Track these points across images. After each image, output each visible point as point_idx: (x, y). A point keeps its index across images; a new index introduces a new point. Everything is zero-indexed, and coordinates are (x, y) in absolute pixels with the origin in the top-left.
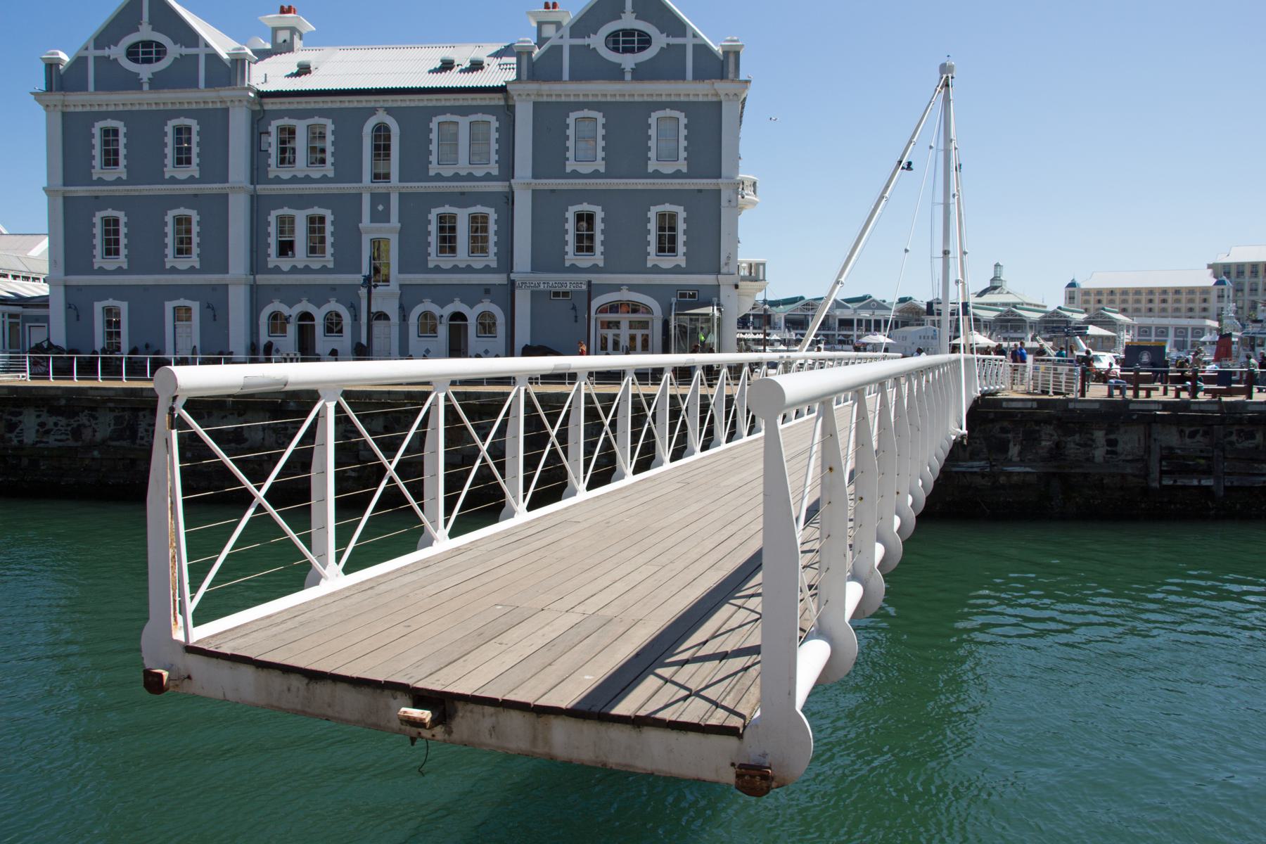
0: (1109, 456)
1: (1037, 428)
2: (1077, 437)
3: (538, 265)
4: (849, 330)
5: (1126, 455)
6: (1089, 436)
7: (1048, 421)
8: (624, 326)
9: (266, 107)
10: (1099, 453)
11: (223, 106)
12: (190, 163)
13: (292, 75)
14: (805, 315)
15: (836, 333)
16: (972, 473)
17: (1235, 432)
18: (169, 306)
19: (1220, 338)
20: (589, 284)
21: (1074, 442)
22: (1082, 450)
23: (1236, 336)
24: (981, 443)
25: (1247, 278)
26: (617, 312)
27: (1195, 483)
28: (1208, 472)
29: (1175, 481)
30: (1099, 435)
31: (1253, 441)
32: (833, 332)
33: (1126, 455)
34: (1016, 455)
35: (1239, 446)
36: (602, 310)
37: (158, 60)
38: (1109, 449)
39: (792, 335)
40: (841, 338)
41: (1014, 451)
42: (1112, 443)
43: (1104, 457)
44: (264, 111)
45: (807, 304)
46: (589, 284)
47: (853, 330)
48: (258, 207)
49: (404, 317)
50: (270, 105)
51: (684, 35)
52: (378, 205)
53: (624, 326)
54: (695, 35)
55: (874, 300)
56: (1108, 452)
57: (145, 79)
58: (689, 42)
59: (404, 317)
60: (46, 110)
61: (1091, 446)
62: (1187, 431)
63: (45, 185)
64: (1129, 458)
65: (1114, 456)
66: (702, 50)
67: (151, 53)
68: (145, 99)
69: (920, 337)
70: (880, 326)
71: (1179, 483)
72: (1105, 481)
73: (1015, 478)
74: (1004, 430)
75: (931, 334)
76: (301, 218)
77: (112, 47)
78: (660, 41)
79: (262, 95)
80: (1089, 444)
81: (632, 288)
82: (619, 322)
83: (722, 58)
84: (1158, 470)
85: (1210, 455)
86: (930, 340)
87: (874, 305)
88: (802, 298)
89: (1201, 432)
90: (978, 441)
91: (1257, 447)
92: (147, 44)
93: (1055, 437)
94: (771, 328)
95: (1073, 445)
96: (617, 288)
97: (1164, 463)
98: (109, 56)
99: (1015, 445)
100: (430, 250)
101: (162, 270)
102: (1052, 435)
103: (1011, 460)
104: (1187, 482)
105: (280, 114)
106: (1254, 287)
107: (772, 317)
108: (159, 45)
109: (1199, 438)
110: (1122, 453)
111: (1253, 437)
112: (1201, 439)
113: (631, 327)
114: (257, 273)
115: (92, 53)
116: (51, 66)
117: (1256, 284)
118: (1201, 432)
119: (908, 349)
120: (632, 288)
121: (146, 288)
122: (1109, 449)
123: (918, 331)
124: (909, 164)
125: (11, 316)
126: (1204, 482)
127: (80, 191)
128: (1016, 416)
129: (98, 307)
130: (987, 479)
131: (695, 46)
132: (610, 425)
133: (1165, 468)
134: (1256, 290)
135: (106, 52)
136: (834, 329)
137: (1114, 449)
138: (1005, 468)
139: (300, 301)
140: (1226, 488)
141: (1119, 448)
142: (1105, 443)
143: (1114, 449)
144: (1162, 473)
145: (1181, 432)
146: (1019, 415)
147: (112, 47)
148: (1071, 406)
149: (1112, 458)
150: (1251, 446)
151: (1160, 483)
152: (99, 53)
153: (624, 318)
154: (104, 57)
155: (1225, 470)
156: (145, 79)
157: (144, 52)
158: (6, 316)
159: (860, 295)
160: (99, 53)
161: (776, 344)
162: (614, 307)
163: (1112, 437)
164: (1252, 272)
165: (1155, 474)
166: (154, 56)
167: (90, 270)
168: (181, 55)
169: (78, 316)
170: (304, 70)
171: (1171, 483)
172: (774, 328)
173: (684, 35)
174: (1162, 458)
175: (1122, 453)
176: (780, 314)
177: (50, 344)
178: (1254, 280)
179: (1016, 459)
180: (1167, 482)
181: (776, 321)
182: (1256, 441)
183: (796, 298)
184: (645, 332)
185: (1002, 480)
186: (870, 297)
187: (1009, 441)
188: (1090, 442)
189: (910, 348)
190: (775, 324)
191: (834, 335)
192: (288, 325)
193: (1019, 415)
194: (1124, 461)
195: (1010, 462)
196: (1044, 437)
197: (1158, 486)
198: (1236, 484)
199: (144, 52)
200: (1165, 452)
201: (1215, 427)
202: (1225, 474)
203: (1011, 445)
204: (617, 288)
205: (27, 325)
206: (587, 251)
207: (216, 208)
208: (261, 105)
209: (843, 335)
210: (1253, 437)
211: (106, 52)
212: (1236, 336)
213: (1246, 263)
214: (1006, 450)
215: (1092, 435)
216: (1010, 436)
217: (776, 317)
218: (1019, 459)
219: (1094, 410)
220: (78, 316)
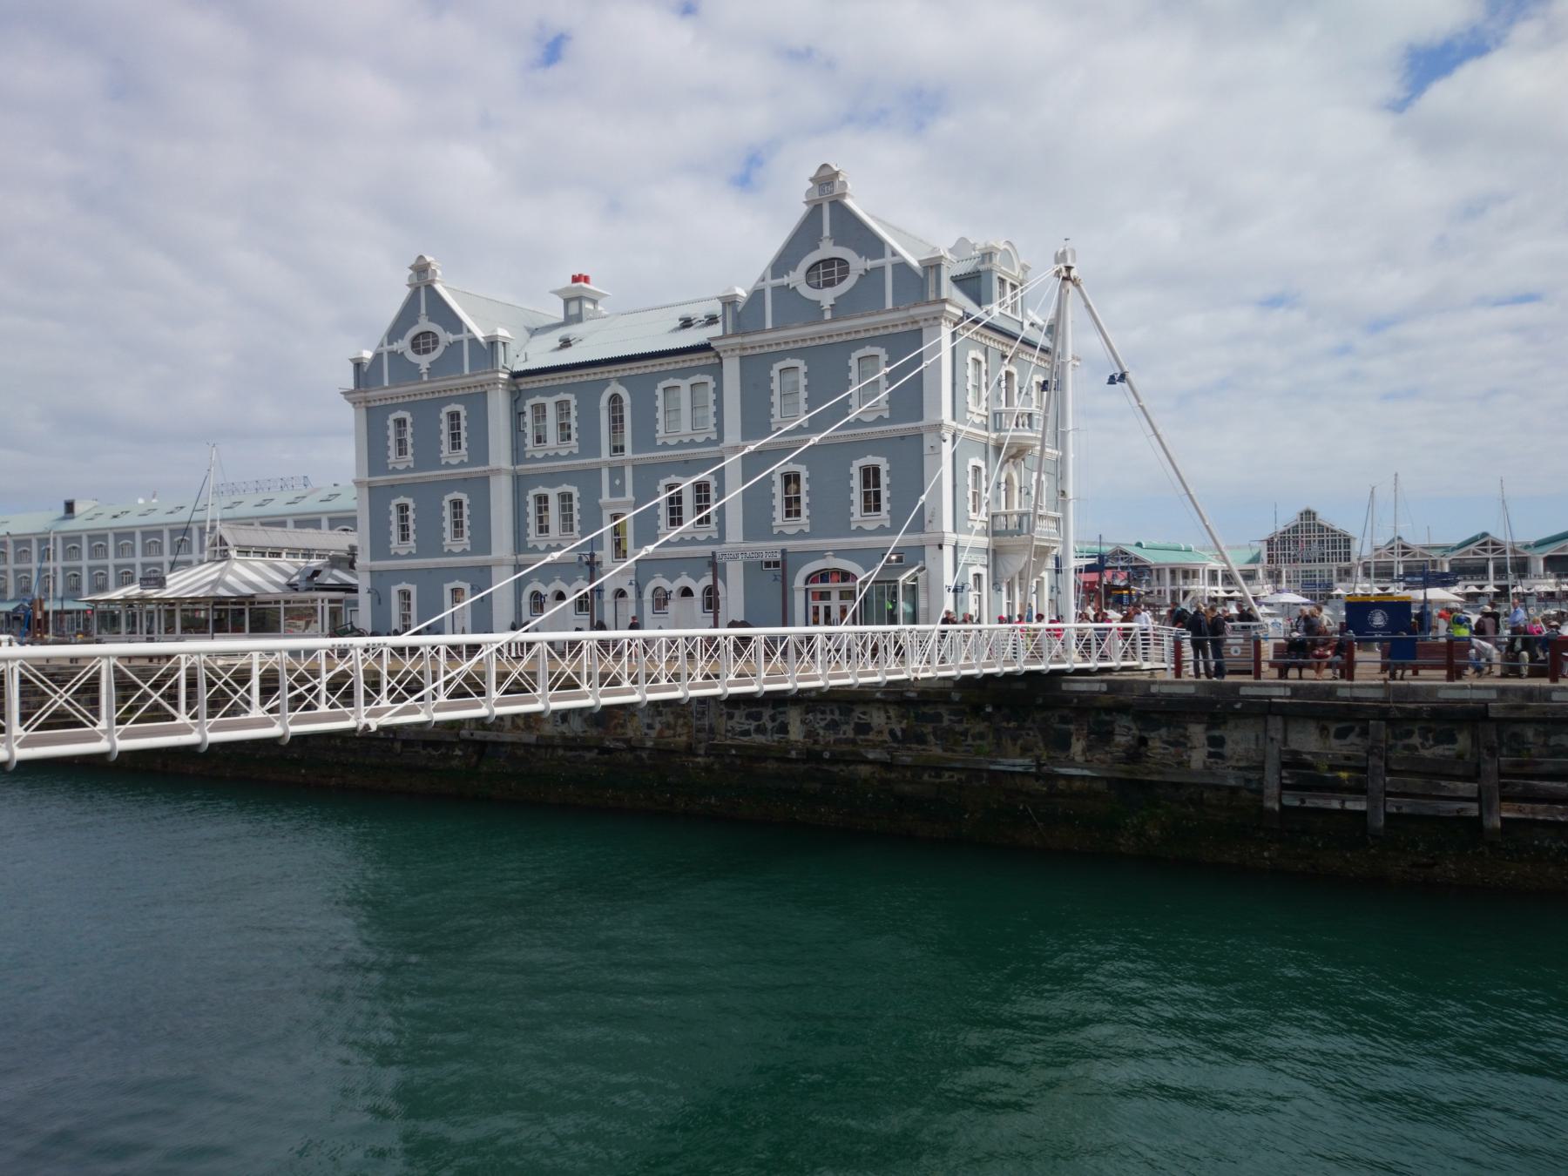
0: (1212, 760)
1: (1107, 718)
2: (1163, 732)
3: (750, 533)
5: (1237, 760)
6: (1181, 730)
7: (1123, 709)
8: (835, 596)
9: (523, 387)
10: (1198, 757)
11: (915, 327)
12: (460, 448)
13: (676, 330)
16: (1012, 773)
17: (1417, 731)
18: (448, 588)
20: (784, 552)
21: (1161, 738)
22: (1172, 750)
24: (1035, 736)
26: (827, 581)
27: (1336, 805)
28: (1358, 790)
29: (1303, 801)
30: (1197, 732)
31: (1450, 746)
33: (1237, 760)
34: (1080, 753)
35: (1426, 753)
36: (811, 578)
37: (841, 280)
38: (1212, 750)
41: (1077, 747)
42: (1216, 742)
43: (1204, 762)
44: (520, 391)
46: (784, 552)
48: (520, 484)
49: (639, 594)
50: (526, 384)
51: (460, 331)
52: (141, 505)
53: (835, 596)
54: (894, 253)
56: (1211, 755)
57: (826, 306)
58: (887, 261)
59: (639, 594)
60: (354, 406)
61: (1184, 745)
62: (1333, 728)
63: (354, 477)
64: (1242, 764)
65: (1219, 761)
66: (902, 268)
67: (832, 273)
68: (425, 387)
71: (1309, 804)
72: (1205, 795)
73: (1077, 784)
74: (1064, 720)
76: (553, 494)
77: (791, 272)
78: (858, 264)
79: (515, 375)
80: (1181, 743)
81: (839, 553)
82: (829, 593)
83: (921, 274)
84: (1276, 783)
85: (1364, 764)
89: (1357, 729)
90: (1031, 733)
91: (1460, 756)
92: (425, 334)
93: (1135, 731)
95: (1158, 744)
96: (820, 554)
97: (1284, 774)
98: (788, 285)
99: (1078, 740)
100: (853, 509)
101: (441, 554)
102: (1130, 729)
103: (1073, 759)
104: (1321, 803)
105: (533, 393)
108: (842, 262)
109: (1352, 738)
110: (1231, 758)
111: (1453, 740)
112: (1357, 741)
113: (841, 598)
114: (520, 553)
115: (771, 282)
116: (358, 365)
118: (1357, 729)
120: (839, 553)
121: (429, 571)
122: (1212, 750)
125: (331, 601)
126: (1349, 806)
127: (380, 479)
128: (1071, 701)
129: (395, 590)
130: (1041, 782)
131: (895, 266)
132: (445, 682)
133: (1288, 782)
135: (785, 280)
137: (1219, 750)
138: (1056, 769)
139: (554, 580)
140: (1388, 816)
141: (1228, 750)
142: (1206, 743)
143: (1219, 750)
144: (1284, 787)
145: (1323, 730)
146: (1075, 700)
147: (791, 272)
148: (1154, 689)
149: (1217, 763)
150: (1447, 753)
151: (1280, 801)
152: (778, 282)
153: (834, 586)
154: (783, 286)
155: (1388, 789)
156: (826, 306)
157: (828, 271)
158: (326, 602)
160: (778, 282)
162: (824, 576)
163: (1216, 733)
165: (1272, 789)
166: (431, 346)
167: (440, 552)
168: (866, 270)
169: (380, 600)
170: (566, 343)
171: (1297, 803)
173: (460, 331)
174: (1284, 765)
175: (1231, 758)
177: (352, 627)
179: (1079, 759)
180: (1291, 801)
182: (1456, 747)
184: (826, 603)
185: (1061, 784)
187: (1071, 734)
188: (1182, 739)
192: (634, 615)
193: (1075, 700)
194: (1234, 768)
195: (1071, 763)
196: (1118, 730)
197: (1277, 807)
198: (1405, 810)
199: (828, 271)
200: (1286, 758)
201: (1371, 722)
202: (1389, 794)
203: (1074, 740)
204: (820, 554)
205: (349, 609)
206: (865, 507)
207: (478, 488)
208: (517, 385)
210: (1453, 740)
211: (785, 280)
214: (1066, 746)
215: (1186, 729)
216: (1072, 727)
218: (1084, 758)
219: (1188, 696)
220: (380, 600)
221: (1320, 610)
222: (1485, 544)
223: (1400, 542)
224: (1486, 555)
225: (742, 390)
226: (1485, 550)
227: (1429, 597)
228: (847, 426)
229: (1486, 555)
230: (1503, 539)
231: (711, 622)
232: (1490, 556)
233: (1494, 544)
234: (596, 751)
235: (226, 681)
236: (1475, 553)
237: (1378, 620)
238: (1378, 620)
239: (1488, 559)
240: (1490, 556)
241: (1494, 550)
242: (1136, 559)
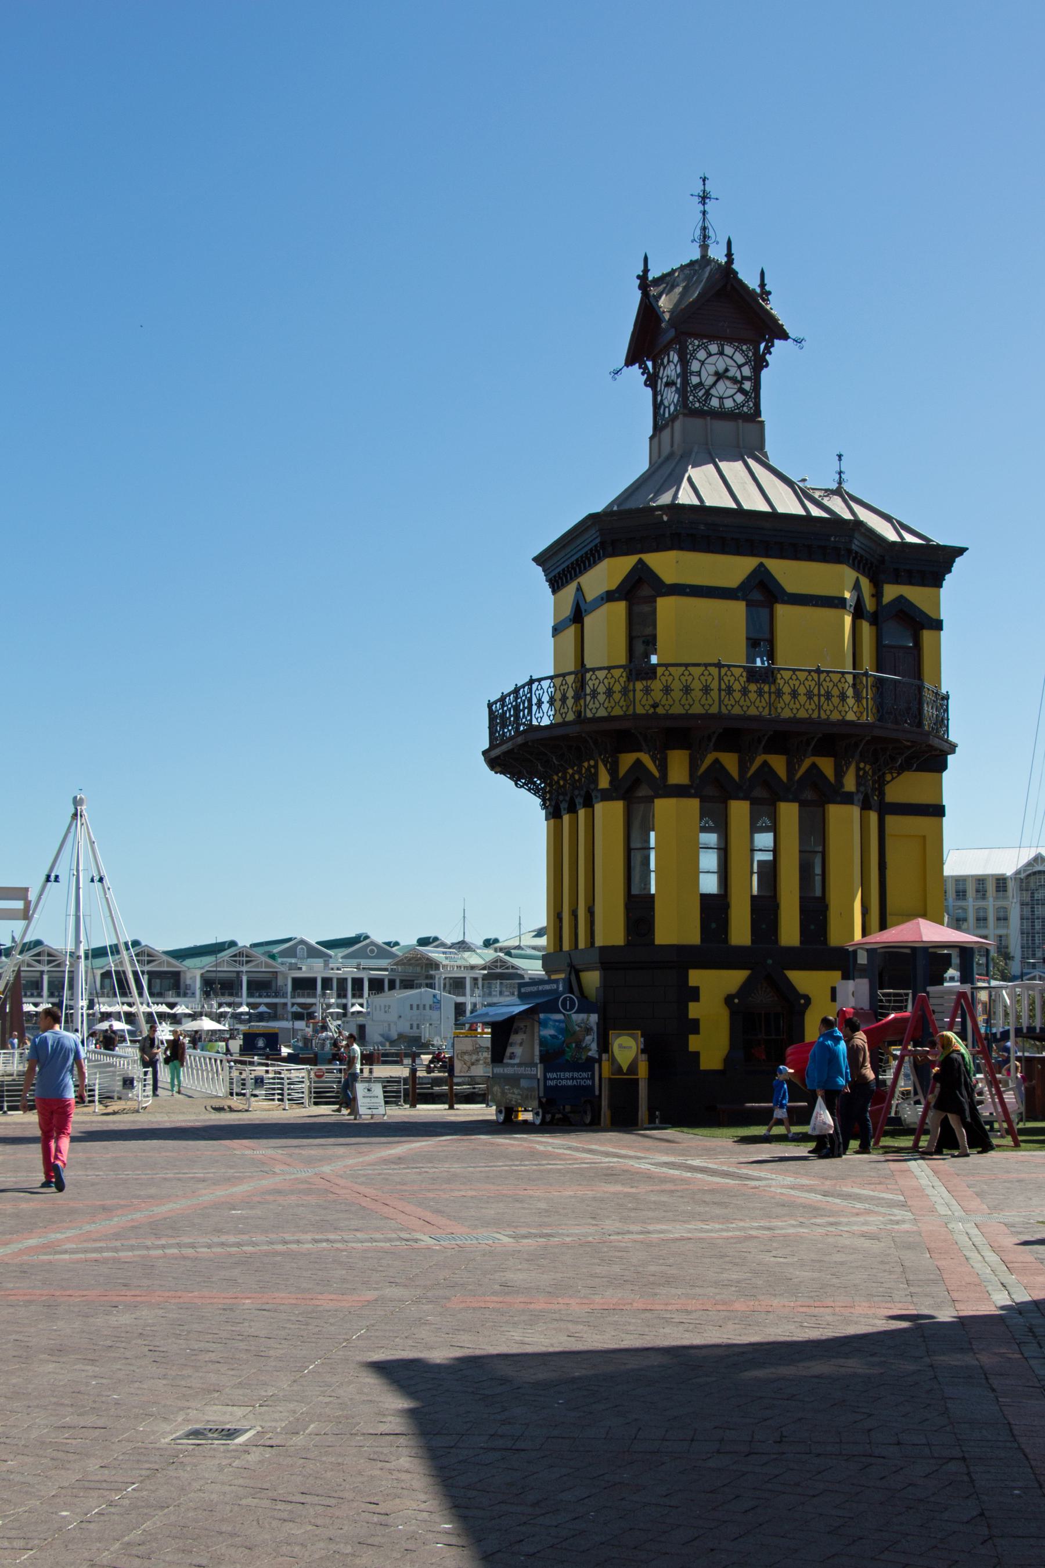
4: (309, 996)
14: (238, 973)
15: (289, 1000)
19: (419, 1055)
23: (952, 979)
25: (971, 900)
32: (283, 1000)
39: (212, 1006)
40: (296, 1009)
45: (240, 954)
47: (314, 996)
55: (373, 944)
69: (411, 1008)
70: (362, 989)
75: (429, 1001)
86: (428, 1011)
87: (372, 951)
88: (233, 944)
94: (178, 995)
106: (981, 914)
107: (182, 975)
117: (985, 909)
119: (392, 1025)
123: (408, 997)
124: (57, 877)
134: (985, 919)
136: (284, 996)
145: (981, 1102)
159: (352, 934)
161: (184, 1020)
164: (977, 891)
172: (185, 995)
176: (194, 971)
178: (981, 903)
181: (188, 982)
183: (224, 943)
186: (367, 937)
189: (396, 1024)
190: (187, 987)
191: (285, 1004)
209: (299, 1004)
212: (952, 979)
213: (988, 875)
217: (189, 975)
221: (174, 1032)
222: (38, 954)
223: (138, 949)
224: (40, 968)
225: (921, 815)
226: (39, 962)
227: (291, 1023)
228: (785, 1093)
229: (40, 968)
230: (183, 963)
231: (920, 823)
232: (46, 968)
233: (49, 955)
234: (812, 1145)
235: (463, 1004)
236: (29, 965)
237: (261, 1043)
238: (261, 1043)
239: (42, 972)
240: (46, 968)
241: (49, 962)
242: (513, 967)
